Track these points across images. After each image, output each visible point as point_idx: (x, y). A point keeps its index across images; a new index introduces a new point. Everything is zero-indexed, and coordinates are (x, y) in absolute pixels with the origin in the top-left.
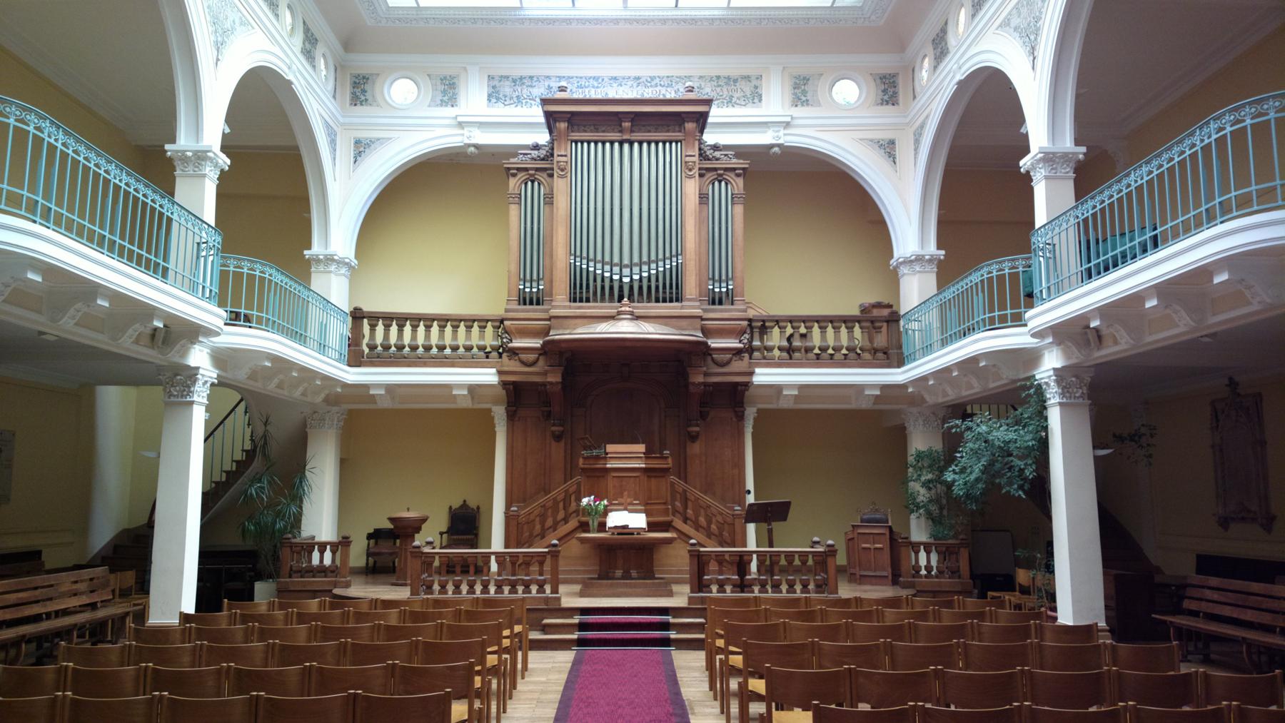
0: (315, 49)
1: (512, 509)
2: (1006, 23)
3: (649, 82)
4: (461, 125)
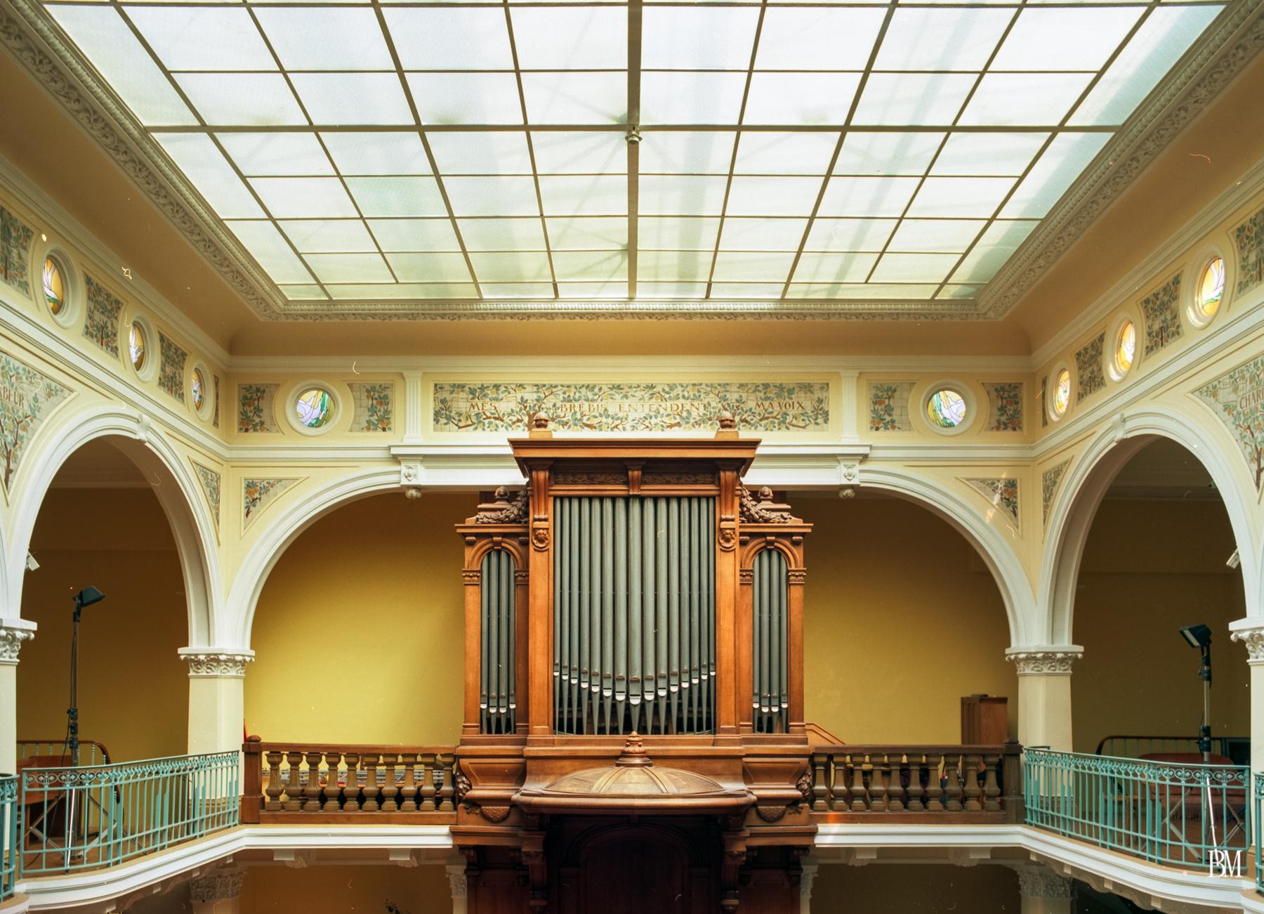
0: (183, 369)
2: (1209, 390)
3: (668, 393)
4: (396, 459)
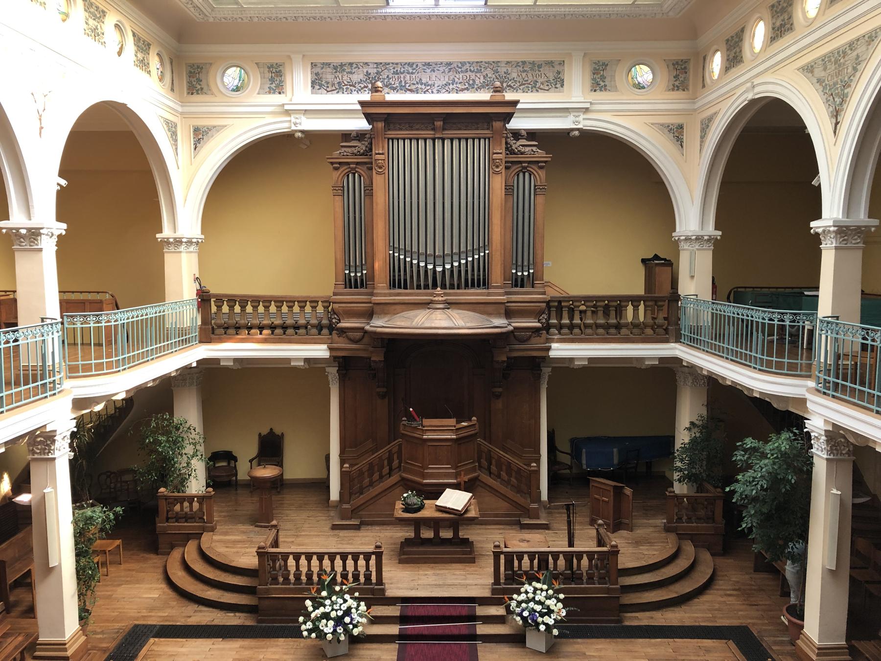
1: (345, 466)
3: (461, 68)
4: (288, 113)
